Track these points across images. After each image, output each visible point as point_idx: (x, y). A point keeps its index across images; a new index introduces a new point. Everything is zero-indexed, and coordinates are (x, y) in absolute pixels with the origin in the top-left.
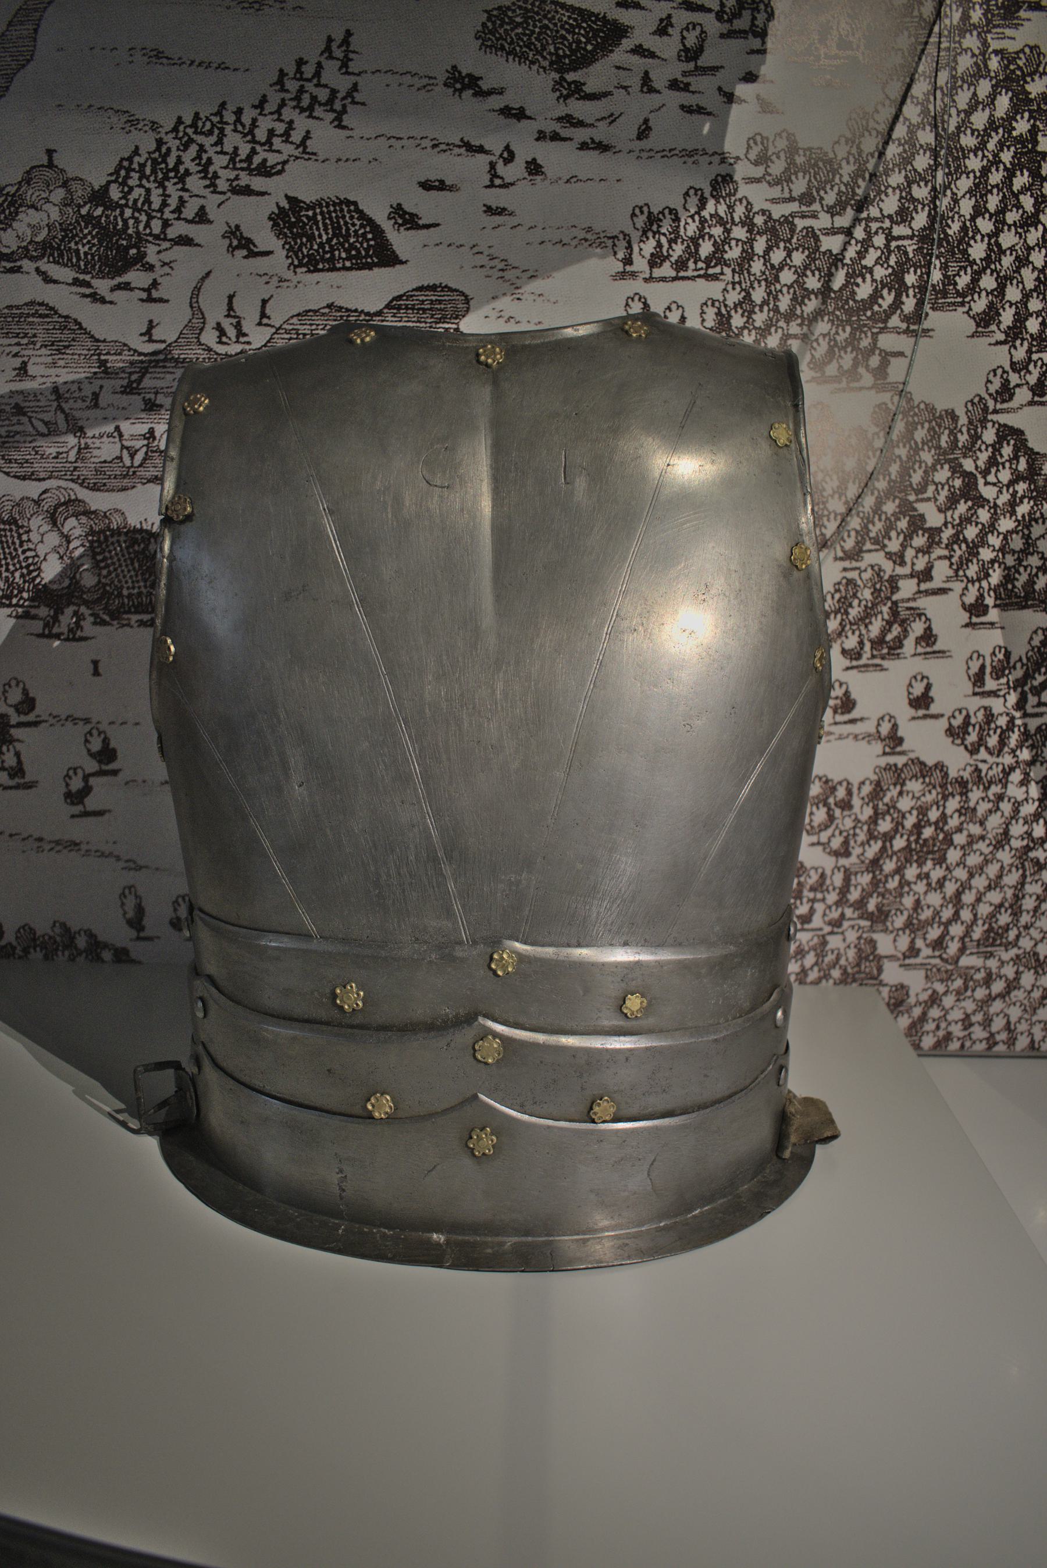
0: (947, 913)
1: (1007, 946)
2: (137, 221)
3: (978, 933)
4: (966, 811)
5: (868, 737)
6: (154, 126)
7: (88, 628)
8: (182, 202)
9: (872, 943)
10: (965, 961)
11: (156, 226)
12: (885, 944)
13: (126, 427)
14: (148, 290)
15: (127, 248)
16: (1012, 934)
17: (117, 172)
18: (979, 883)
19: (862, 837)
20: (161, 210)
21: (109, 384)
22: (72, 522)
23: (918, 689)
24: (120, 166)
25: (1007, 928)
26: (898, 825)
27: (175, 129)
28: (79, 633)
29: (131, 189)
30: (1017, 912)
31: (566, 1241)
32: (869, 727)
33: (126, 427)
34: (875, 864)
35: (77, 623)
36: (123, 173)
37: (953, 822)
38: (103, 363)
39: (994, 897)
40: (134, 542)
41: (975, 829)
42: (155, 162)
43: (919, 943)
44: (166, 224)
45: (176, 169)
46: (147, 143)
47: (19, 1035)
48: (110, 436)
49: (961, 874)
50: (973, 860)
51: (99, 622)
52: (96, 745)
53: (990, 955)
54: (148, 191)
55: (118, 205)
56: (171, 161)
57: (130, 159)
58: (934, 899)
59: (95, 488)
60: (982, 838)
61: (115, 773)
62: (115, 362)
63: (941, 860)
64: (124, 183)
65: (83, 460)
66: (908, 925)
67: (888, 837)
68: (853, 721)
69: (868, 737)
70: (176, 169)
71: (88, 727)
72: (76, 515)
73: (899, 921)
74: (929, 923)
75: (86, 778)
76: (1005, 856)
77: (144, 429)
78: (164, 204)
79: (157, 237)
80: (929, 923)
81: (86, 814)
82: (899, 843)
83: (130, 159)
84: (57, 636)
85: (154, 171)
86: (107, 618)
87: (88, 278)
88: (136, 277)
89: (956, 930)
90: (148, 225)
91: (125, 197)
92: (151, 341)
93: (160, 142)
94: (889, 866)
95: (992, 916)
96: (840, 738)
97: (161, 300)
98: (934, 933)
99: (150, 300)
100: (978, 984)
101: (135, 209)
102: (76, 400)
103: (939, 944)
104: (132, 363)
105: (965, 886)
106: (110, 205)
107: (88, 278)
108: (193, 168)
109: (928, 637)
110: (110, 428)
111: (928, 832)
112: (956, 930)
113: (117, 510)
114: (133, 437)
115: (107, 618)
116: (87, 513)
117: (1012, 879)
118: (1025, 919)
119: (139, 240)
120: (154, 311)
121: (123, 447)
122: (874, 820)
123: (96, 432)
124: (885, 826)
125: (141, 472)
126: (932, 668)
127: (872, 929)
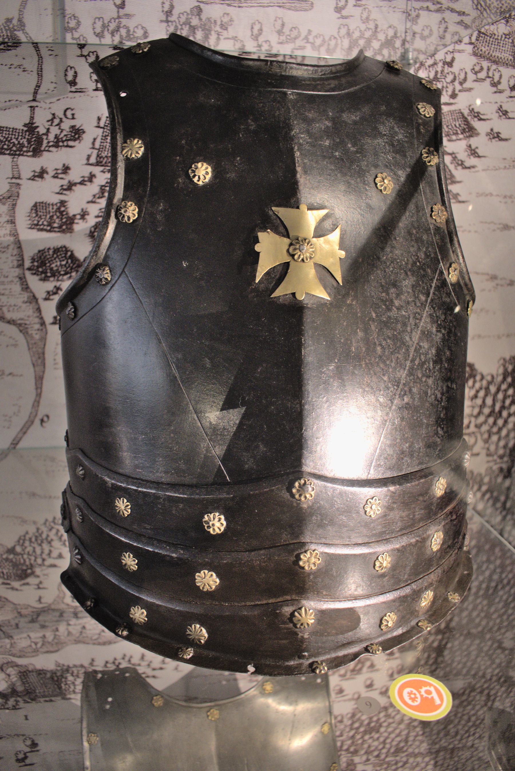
0: (381, 747)
1: (404, 752)
2: (30, 559)
3: (392, 750)
4: (388, 716)
5: (350, 700)
6: (35, 523)
7: (21, 704)
8: (50, 551)
9: (352, 760)
10: (388, 759)
11: (39, 561)
12: (357, 759)
13: (32, 635)
14: (38, 585)
15: (26, 570)
16: (405, 749)
17: (19, 541)
18: (393, 736)
19: (348, 729)
20: (41, 555)
21: (22, 620)
22: (11, 669)
23: (368, 682)
24: (20, 539)
25: (403, 747)
26: (361, 725)
27: (45, 524)
28: (17, 707)
29: (26, 547)
30: (406, 741)
31: (318, 613)
32: (350, 697)
33: (32, 635)
34: (353, 737)
35: (17, 704)
36: (21, 541)
37: (382, 720)
38: (19, 613)
39: (398, 739)
40: (40, 674)
41: (391, 720)
42: (36, 537)
43: (370, 757)
44: (44, 560)
45: (47, 539)
46: (32, 530)
47: (83, 292)
48: (25, 638)
49: (386, 734)
50: (390, 729)
51: (26, 702)
52: (29, 742)
53: (396, 756)
54: (34, 548)
55: (20, 554)
56: (44, 536)
57: (25, 536)
58: (376, 743)
59: (20, 657)
60: (393, 723)
61: (38, 751)
62: (24, 612)
63: (378, 732)
64: (22, 545)
65: (14, 647)
66: (366, 753)
67: (358, 728)
68: (343, 696)
69: (350, 700)
70: (47, 539)
71: (24, 737)
72: (12, 667)
73: (363, 752)
74: (374, 751)
75: (25, 754)
76: (402, 726)
77: (40, 634)
78: (42, 552)
79: (40, 565)
80: (374, 751)
81: (26, 765)
82: (362, 729)
83: (25, 536)
84: (8, 709)
85: (36, 540)
86: (29, 701)
87: (8, 582)
88: (31, 580)
89: (384, 751)
90: (35, 560)
91: (23, 550)
92: (41, 603)
93: (38, 529)
94: (358, 737)
95: (398, 745)
96: (339, 702)
97: (44, 588)
98: (376, 753)
99: (39, 588)
100: (393, 765)
101: (28, 554)
102: (8, 626)
103: (378, 756)
104: (33, 612)
105: (387, 738)
106: (16, 554)
107: (8, 582)
108: (55, 538)
109: (372, 666)
110: (25, 635)
111: (373, 724)
112: (384, 751)
113: (31, 664)
114: (36, 638)
115: (29, 701)
116: (17, 666)
117: (404, 733)
118: (410, 743)
119: (32, 566)
120: (40, 592)
121: (32, 642)
122: (352, 724)
123: (18, 637)
124: (356, 725)
125: (41, 650)
126: (374, 675)
127: (352, 756)
